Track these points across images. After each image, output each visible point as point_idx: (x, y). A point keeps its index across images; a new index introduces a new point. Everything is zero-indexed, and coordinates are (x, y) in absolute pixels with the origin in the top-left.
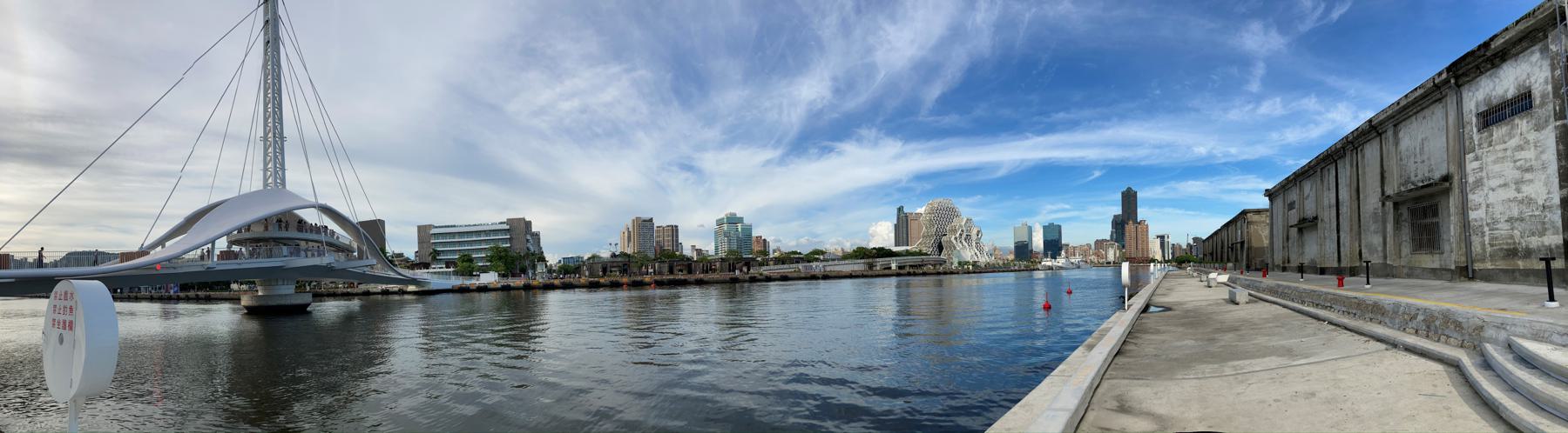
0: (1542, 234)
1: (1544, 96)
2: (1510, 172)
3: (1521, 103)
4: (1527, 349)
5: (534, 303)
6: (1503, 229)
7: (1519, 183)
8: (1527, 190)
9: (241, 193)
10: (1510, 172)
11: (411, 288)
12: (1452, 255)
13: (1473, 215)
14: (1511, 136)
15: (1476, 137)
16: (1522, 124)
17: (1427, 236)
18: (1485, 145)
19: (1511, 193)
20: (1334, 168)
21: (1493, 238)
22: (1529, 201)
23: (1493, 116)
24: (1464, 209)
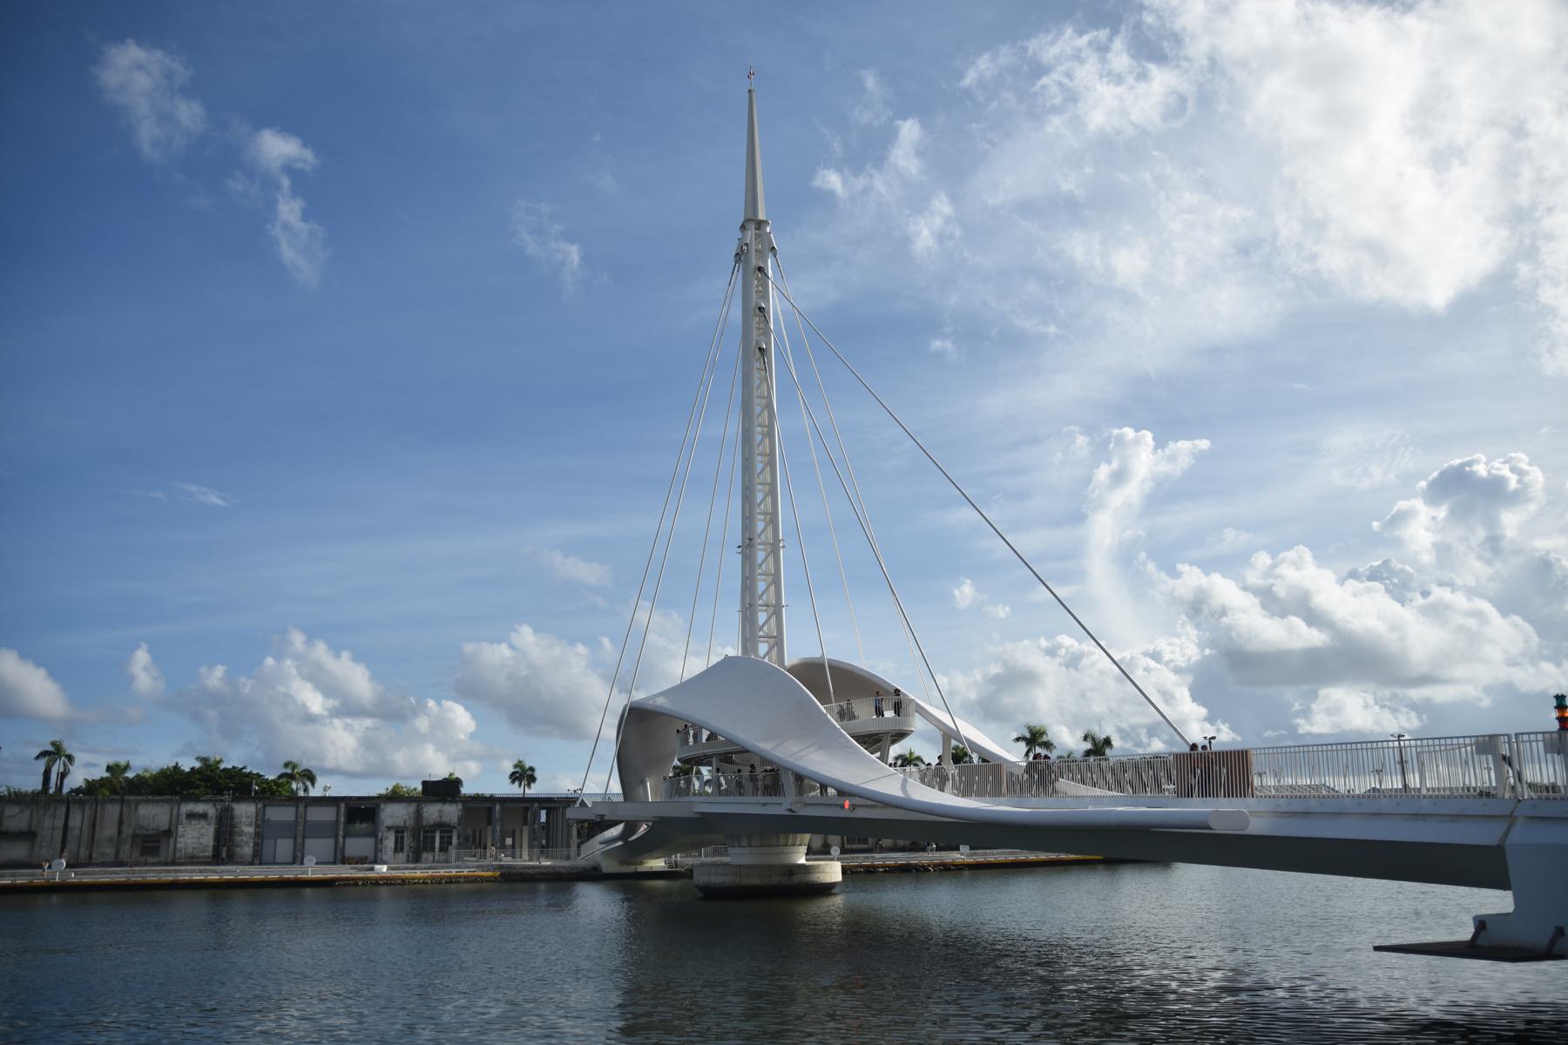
0: (204, 852)
1: (212, 817)
2: (196, 834)
3: (204, 816)
4: (867, 789)
5: (516, 631)
6: (190, 850)
7: (198, 838)
8: (201, 840)
9: (683, 680)
10: (196, 834)
11: (351, 882)
12: (162, 857)
13: (178, 845)
14: (198, 824)
15: (184, 821)
16: (203, 822)
17: (155, 851)
18: (1138, 925)
19: (196, 840)
20: (64, 809)
21: (185, 854)
22: (201, 843)
23: (191, 816)
24: (175, 843)
